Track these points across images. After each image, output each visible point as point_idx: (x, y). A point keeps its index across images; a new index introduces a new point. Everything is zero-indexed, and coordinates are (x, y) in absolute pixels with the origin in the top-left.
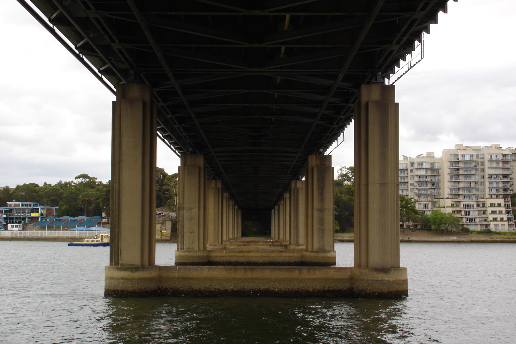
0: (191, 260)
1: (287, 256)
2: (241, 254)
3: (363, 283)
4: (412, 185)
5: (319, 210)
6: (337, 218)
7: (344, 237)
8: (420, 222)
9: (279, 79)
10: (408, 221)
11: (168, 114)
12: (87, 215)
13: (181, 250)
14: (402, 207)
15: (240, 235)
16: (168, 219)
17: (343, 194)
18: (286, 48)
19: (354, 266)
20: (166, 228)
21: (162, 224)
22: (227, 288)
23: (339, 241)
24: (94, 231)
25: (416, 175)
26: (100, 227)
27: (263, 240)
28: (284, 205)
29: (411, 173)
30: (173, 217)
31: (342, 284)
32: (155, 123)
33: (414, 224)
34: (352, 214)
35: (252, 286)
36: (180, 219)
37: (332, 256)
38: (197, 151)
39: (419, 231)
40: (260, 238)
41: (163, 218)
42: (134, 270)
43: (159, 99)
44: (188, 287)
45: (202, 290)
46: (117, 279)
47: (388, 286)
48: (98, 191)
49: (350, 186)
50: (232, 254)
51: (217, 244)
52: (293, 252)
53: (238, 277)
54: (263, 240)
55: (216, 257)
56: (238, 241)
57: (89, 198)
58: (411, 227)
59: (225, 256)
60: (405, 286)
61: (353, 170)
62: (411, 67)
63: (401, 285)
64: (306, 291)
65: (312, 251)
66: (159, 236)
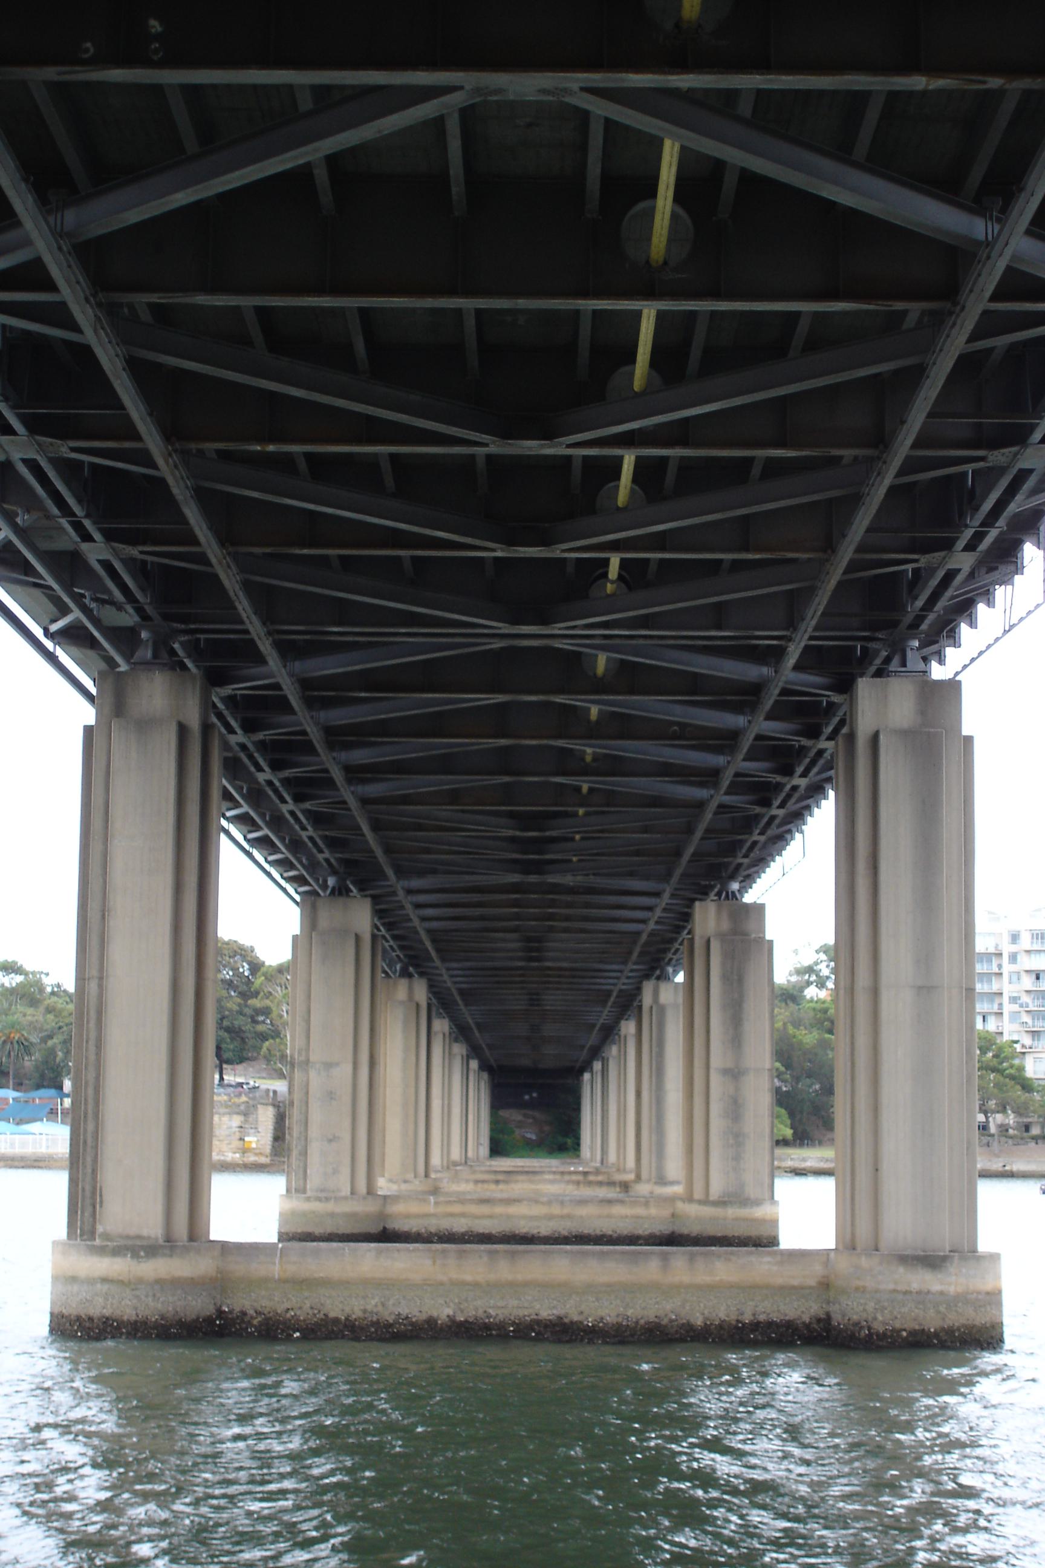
0: (329, 1228)
1: (627, 1217)
2: (485, 1209)
3: (862, 1301)
4: (1014, 1000)
5: (724, 1071)
6: (782, 1099)
7: (804, 1160)
8: (1040, 1116)
9: (602, 662)
10: (1003, 1109)
11: (260, 769)
12: (18, 1086)
13: (298, 1195)
14: (985, 1068)
15: (485, 1150)
16: (263, 1101)
17: (802, 1028)
18: (624, 563)
19: (833, 1247)
20: (256, 1128)
21: (246, 1114)
22: (435, 1314)
23: (791, 1172)
24: (38, 1137)
25: (1027, 971)
26: (54, 1124)
27: (557, 1167)
28: (620, 1059)
29: (1011, 965)
30: (278, 1093)
31: (795, 1303)
32: (215, 794)
33: (1021, 1120)
34: (829, 1090)
35: (513, 1307)
36: (297, 1097)
37: (768, 1217)
38: (351, 887)
39: (1037, 1143)
40: (547, 1161)
41: (249, 1098)
42: (142, 1254)
43: (233, 723)
44: (312, 1308)
45: (355, 1320)
46: (91, 1281)
47: (942, 1309)
48: (50, 1012)
49: (824, 1002)
50: (457, 1209)
51: (410, 1176)
52: (646, 1204)
53: (468, 1278)
54: (557, 1167)
55: (408, 1216)
56: (477, 1168)
57: (23, 1035)
58: (1011, 1131)
59: (434, 1215)
60: (994, 1312)
61: (832, 954)
62: (1012, 627)
63: (980, 1306)
64: (683, 1324)
65: (705, 1202)
66: (235, 1153)
